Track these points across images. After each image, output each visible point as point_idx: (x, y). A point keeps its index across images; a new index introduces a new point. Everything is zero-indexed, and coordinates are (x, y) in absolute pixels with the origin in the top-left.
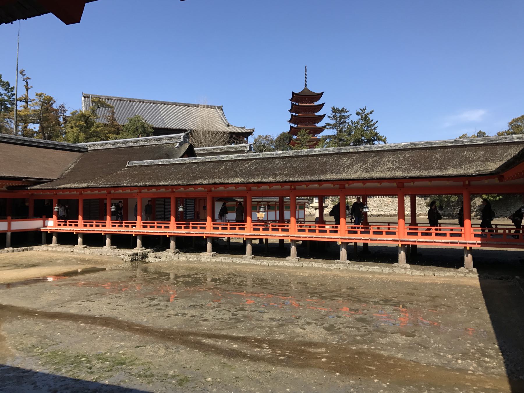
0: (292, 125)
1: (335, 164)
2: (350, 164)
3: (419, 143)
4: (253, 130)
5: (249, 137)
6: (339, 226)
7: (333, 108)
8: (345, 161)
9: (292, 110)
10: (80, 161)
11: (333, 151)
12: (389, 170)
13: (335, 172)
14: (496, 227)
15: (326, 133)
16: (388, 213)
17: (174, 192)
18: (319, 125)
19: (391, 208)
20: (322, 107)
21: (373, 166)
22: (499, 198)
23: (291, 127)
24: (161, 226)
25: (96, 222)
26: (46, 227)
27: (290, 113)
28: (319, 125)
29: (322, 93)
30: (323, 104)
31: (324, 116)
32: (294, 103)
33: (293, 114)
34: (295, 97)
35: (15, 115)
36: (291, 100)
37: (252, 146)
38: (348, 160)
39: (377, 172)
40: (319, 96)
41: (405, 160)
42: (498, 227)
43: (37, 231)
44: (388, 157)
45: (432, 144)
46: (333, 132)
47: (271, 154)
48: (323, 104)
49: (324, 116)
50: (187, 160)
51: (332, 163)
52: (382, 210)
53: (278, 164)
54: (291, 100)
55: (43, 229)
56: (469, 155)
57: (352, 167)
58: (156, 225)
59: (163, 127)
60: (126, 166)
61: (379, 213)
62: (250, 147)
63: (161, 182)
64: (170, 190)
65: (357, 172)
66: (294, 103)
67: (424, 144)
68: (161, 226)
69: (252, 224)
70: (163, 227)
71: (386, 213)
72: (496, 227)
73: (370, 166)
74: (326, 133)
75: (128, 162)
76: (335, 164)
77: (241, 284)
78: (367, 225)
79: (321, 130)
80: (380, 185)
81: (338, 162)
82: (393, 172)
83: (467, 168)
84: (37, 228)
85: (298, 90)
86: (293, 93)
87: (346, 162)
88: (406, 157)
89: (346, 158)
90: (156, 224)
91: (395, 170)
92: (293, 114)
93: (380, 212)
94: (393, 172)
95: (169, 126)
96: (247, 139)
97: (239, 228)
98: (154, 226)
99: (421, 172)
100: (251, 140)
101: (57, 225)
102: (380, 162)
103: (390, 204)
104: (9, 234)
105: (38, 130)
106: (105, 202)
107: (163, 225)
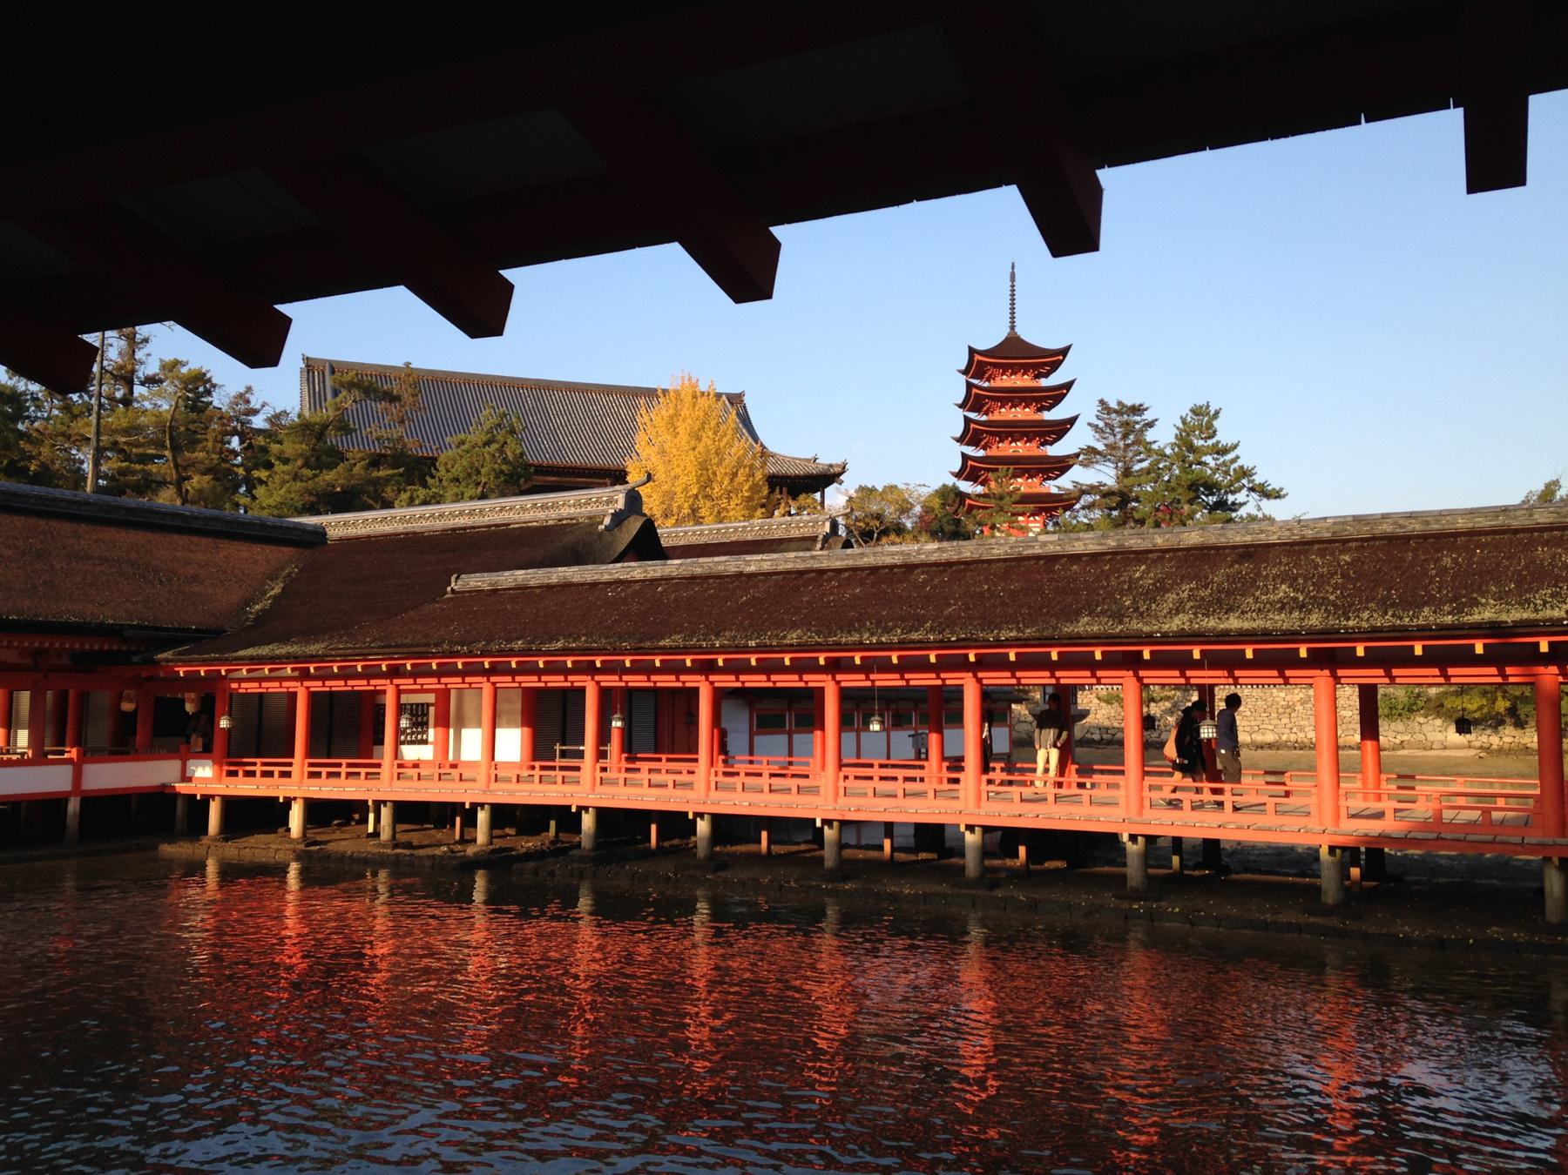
0: (970, 451)
1: (1108, 586)
2: (1154, 584)
3: (1385, 517)
5: (830, 491)
7: (1102, 402)
8: (1138, 575)
10: (301, 571)
11: (1102, 544)
12: (1282, 608)
13: (1107, 611)
16: (1293, 737)
19: (1302, 723)
21: (1229, 593)
23: (965, 457)
24: (320, 773)
26: (189, 780)
27: (960, 413)
29: (1064, 352)
30: (1068, 386)
31: (1072, 421)
32: (976, 382)
34: (978, 364)
35: (93, 429)
37: (840, 520)
38: (1147, 571)
39: (1243, 613)
41: (1336, 573)
43: (162, 793)
44: (1280, 563)
45: (1427, 523)
46: (1105, 475)
47: (901, 553)
48: (1068, 386)
49: (1072, 421)
50: (636, 571)
51: (1098, 580)
52: (1271, 727)
53: (925, 582)
54: (965, 372)
55: (182, 788)
56: (1553, 558)
57: (1163, 596)
60: (449, 589)
62: (834, 525)
63: (558, 640)
65: (1178, 612)
66: (976, 382)
67: (1401, 522)
68: (320, 773)
71: (1284, 738)
73: (1219, 592)
75: (455, 576)
76: (1108, 586)
79: (1061, 466)
81: (1118, 578)
82: (1296, 614)
83: (1545, 603)
84: (163, 786)
86: (972, 351)
87: (1141, 578)
88: (1339, 564)
89: (1143, 567)
90: (344, 766)
91: (1303, 606)
92: (972, 415)
94: (1296, 614)
95: (575, 459)
96: (823, 496)
97: (367, 774)
99: (1390, 613)
100: (835, 498)
102: (1254, 581)
103: (1299, 707)
104: (73, 805)
105: (1224, 849)
106: (379, 700)
107: (324, 770)
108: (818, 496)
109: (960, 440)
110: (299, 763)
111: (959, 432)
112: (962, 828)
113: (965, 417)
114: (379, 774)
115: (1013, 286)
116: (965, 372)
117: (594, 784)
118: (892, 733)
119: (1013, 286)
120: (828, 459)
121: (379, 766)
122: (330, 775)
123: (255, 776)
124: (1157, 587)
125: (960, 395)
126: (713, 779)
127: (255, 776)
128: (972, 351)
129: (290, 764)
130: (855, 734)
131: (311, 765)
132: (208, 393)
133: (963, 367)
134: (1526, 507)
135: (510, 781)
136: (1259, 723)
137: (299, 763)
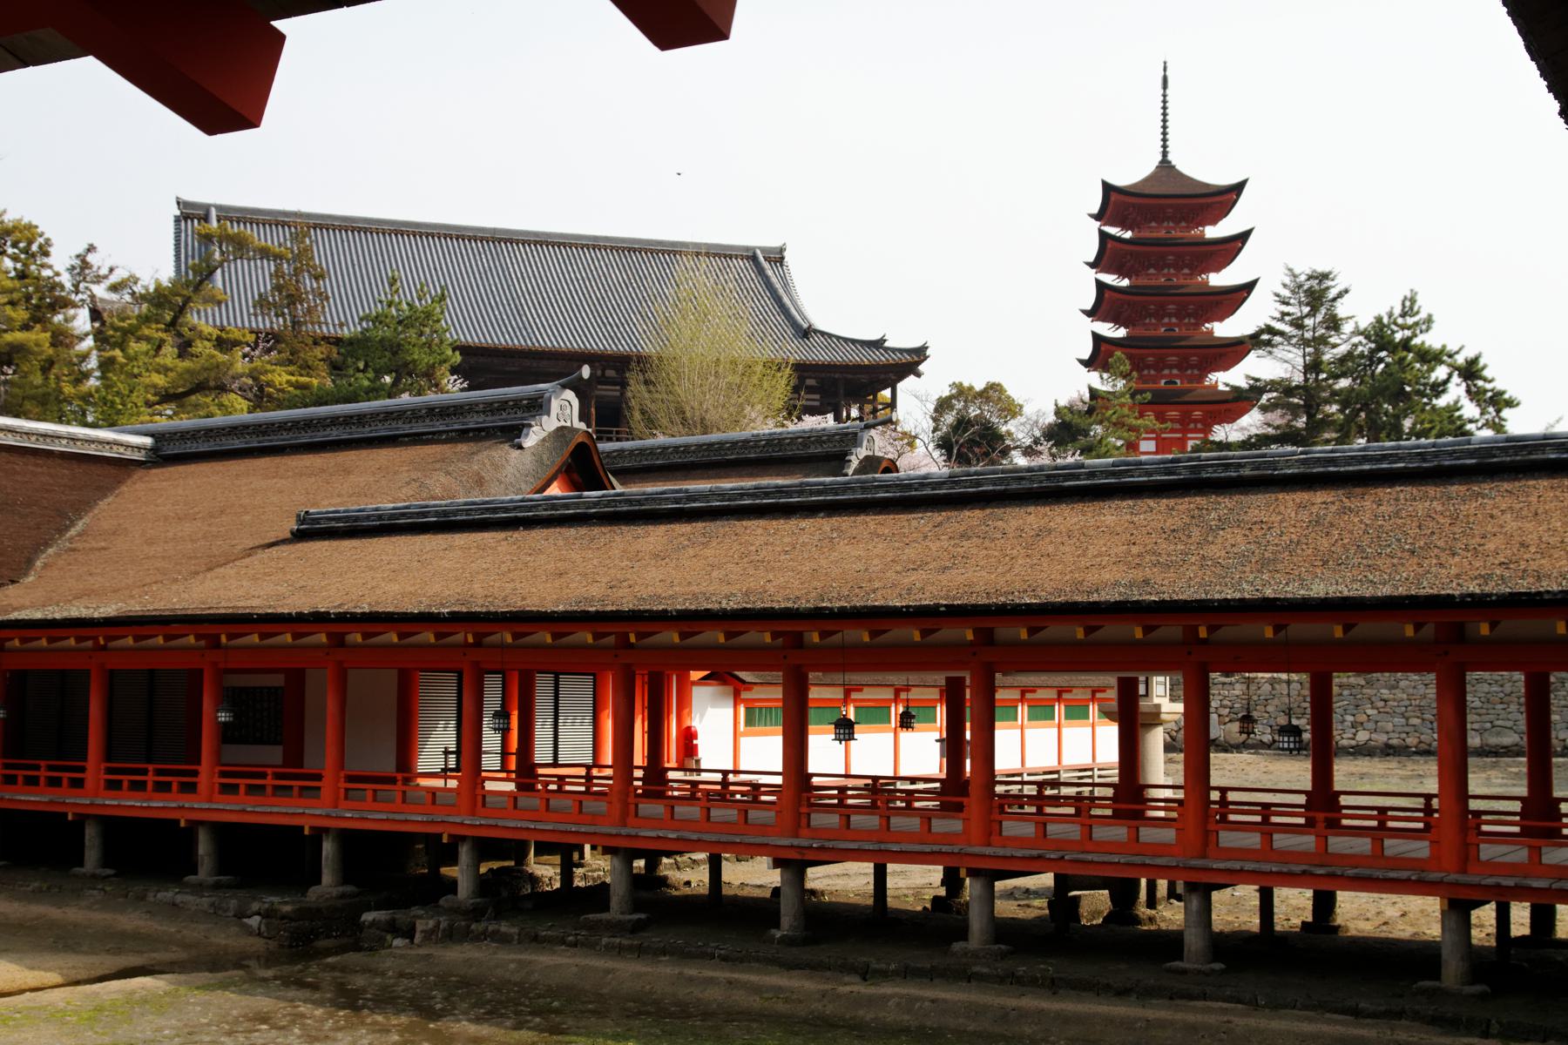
4: (920, 353)
5: (907, 386)
6: (965, 800)
9: (1103, 263)
14: (1223, 796)
15: (1255, 367)
17: (631, 646)
18: (1226, 329)
20: (1240, 250)
22: (496, 927)
25: (50, 768)
27: (1091, 274)
28: (1226, 329)
29: (1239, 188)
30: (1244, 237)
31: (1249, 287)
33: (1109, 279)
36: (1097, 217)
40: (1225, 198)
42: (1232, 796)
48: (1244, 237)
49: (1249, 287)
52: (1509, 724)
54: (1097, 217)
58: (150, 778)
59: (519, 341)
61: (1493, 740)
64: (611, 640)
68: (120, 782)
69: (218, 769)
70: (175, 787)
72: (1223, 796)
74: (1255, 367)
77: (1382, 751)
78: (529, 777)
79: (1235, 350)
80: (1491, 631)
85: (1133, 171)
86: (1107, 188)
93: (1498, 734)
97: (302, 788)
98: (145, 783)
101: (102, 782)
108: (887, 393)
109: (1092, 313)
110: (94, 767)
111: (1089, 301)
112: (963, 873)
113: (1100, 285)
114: (319, 788)
115: (1165, 96)
116: (1097, 217)
117: (475, 805)
118: (1028, 732)
119: (1165, 96)
120: (900, 339)
121: (83, 769)
122: (251, 789)
123: (16, 783)
124: (366, 366)
125: (1091, 250)
126: (343, 785)
127: (16, 783)
128: (1107, 188)
129: (83, 769)
130: (892, 735)
131: (7, 766)
132: (73, 268)
133: (1095, 210)
134: (1131, 186)
135: (365, 801)
136: (1492, 717)
137: (94, 767)
